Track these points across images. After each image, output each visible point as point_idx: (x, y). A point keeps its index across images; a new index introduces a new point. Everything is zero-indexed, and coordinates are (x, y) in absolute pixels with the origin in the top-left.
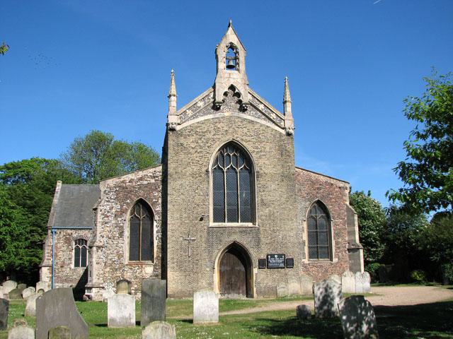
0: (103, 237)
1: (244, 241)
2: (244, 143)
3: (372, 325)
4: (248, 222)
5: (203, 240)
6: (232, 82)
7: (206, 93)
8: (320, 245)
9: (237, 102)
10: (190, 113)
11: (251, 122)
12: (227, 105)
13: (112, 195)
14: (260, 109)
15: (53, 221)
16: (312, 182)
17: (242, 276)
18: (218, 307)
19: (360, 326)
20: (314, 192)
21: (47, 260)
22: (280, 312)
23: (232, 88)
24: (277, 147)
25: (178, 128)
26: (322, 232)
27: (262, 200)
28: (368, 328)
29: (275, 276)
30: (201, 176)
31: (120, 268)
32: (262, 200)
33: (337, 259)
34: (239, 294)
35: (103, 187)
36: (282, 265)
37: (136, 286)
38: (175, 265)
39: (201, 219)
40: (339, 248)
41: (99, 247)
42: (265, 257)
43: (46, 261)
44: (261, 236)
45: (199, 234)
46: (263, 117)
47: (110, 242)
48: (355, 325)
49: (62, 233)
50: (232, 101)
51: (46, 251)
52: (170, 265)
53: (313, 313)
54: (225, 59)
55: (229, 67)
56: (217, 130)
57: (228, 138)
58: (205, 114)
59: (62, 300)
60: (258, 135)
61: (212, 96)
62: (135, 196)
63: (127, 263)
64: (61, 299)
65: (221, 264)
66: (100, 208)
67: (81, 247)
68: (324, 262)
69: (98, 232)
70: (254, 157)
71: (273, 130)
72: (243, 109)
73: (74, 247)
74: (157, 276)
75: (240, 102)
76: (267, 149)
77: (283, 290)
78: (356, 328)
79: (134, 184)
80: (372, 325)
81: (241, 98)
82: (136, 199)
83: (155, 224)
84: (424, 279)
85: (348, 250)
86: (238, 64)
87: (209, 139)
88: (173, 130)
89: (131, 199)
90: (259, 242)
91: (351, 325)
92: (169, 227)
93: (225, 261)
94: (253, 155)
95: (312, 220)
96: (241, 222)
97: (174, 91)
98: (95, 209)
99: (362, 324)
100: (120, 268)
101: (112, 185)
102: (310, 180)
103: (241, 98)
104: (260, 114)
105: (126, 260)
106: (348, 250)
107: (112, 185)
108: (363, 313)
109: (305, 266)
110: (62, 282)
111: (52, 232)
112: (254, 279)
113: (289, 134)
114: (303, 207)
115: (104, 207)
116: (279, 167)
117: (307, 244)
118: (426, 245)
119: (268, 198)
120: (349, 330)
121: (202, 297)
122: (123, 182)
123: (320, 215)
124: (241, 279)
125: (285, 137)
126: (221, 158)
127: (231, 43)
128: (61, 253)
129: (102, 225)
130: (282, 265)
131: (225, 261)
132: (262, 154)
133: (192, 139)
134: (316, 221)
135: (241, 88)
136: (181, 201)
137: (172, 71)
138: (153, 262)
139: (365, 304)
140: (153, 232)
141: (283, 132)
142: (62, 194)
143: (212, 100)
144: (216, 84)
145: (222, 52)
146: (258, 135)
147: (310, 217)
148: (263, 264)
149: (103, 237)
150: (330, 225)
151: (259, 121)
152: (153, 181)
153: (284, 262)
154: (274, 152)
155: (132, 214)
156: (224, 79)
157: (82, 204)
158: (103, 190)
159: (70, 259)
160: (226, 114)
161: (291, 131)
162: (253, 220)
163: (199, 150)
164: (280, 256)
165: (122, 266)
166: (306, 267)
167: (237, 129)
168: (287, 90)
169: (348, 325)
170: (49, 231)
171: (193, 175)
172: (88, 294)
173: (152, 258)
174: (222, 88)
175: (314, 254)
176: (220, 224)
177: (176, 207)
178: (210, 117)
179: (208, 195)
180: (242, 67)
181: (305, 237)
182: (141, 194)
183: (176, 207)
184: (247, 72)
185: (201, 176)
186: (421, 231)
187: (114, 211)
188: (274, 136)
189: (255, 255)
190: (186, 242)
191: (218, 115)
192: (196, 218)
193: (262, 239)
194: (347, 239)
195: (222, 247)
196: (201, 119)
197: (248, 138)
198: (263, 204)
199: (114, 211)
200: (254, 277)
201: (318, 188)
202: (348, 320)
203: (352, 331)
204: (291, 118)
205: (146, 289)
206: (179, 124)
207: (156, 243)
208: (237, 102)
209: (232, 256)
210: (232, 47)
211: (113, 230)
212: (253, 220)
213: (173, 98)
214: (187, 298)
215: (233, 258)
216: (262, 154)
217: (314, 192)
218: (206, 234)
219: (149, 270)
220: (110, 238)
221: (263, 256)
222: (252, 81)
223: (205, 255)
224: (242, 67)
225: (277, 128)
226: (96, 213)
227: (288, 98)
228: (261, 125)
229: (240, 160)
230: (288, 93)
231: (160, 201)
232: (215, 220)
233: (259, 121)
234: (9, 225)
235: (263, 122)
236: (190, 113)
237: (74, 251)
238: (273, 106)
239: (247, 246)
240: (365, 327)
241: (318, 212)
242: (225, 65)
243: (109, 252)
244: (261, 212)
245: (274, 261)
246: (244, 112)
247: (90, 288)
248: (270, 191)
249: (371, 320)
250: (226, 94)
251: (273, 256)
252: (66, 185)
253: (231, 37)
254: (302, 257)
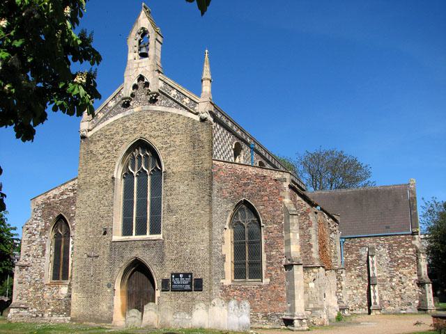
1: (147, 257)
6: (140, 72)
11: (162, 113)
14: (171, 96)
16: (238, 177)
20: (240, 190)
23: (141, 78)
24: (189, 139)
25: (89, 134)
27: (169, 206)
29: (180, 301)
32: (169, 206)
33: (268, 280)
37: (52, 307)
38: (78, 285)
39: (105, 233)
41: (22, 267)
42: (170, 277)
44: (166, 251)
46: (175, 104)
56: (125, 129)
57: (137, 136)
76: (178, 143)
77: (133, 319)
82: (56, 215)
90: (163, 259)
97: (207, 74)
104: (171, 101)
107: (40, 203)
109: (223, 288)
114: (224, 209)
116: (190, 163)
119: (175, 203)
122: (48, 198)
125: (200, 124)
127: (143, 28)
129: (29, 243)
130: (188, 287)
132: (171, 149)
133: (101, 144)
141: (197, 118)
145: (133, 41)
148: (166, 285)
149: (29, 256)
151: (170, 110)
153: (190, 283)
160: (136, 110)
163: (107, 155)
164: (186, 275)
166: (225, 290)
171: (100, 184)
177: (83, 221)
183: (83, 221)
188: (186, 125)
189: (158, 275)
191: (128, 112)
193: (167, 254)
195: (123, 265)
197: (157, 133)
198: (170, 210)
201: (245, 184)
206: (89, 130)
209: (142, 275)
214: (88, 323)
216: (171, 149)
217: (240, 190)
221: (167, 276)
222: (165, 67)
228: (173, 115)
233: (170, 110)
235: (175, 111)
244: (166, 221)
245: (179, 282)
246: (154, 103)
250: (135, 87)
251: (177, 275)
253: (144, 21)
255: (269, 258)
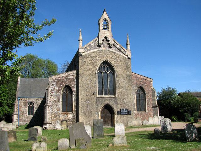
0: (51, 101)
1: (112, 103)
2: (111, 62)
3: (196, 135)
4: (112, 95)
5: (94, 103)
7: (95, 40)
8: (141, 105)
9: (108, 44)
10: (88, 48)
12: (104, 45)
13: (54, 83)
14: (117, 47)
15: (18, 94)
17: (110, 118)
18: (124, 130)
19: (192, 135)
21: (16, 112)
22: (145, 131)
23: (106, 38)
25: (83, 54)
26: (142, 100)
27: (118, 86)
28: (195, 136)
30: (93, 75)
31: (58, 115)
33: (148, 111)
34: (109, 126)
35: (50, 80)
36: (127, 113)
39: (93, 94)
40: (149, 106)
41: (49, 106)
42: (120, 110)
43: (15, 112)
45: (93, 100)
46: (119, 51)
47: (54, 104)
48: (190, 135)
49: (22, 99)
50: (106, 44)
51: (16, 108)
52: (80, 114)
53: (167, 130)
54: (102, 25)
55: (104, 29)
56: (99, 56)
57: (104, 59)
58: (94, 49)
59: (80, 128)
60: (116, 58)
61: (97, 41)
62: (64, 83)
63: (61, 113)
64: (79, 127)
65: (101, 113)
66: (49, 89)
67: (31, 106)
68: (143, 112)
69: (49, 99)
70: (115, 67)
71: (122, 56)
72: (110, 47)
73: (28, 106)
74: (74, 118)
75: (109, 44)
77: (130, 124)
78: (191, 136)
79: (64, 78)
80: (196, 135)
81: (109, 42)
83: (73, 96)
84: (177, 119)
85: (152, 107)
86: (108, 27)
87: (96, 59)
88: (81, 55)
89: (63, 85)
91: (189, 135)
92: (80, 97)
93: (103, 112)
94: (115, 67)
95: (138, 94)
96: (110, 95)
97: (81, 38)
98: (48, 89)
99: (193, 134)
100: (58, 115)
101: (54, 79)
102: (137, 77)
103: (109, 42)
104: (117, 49)
105: (61, 112)
106: (152, 107)
107: (54, 79)
108: (193, 130)
109: (135, 114)
110: (23, 121)
111: (18, 99)
112: (115, 119)
113: (129, 58)
114: (135, 89)
115: (51, 88)
117: (136, 104)
118: (178, 105)
120: (188, 136)
121: (118, 126)
122: (59, 77)
123: (141, 92)
124: (110, 119)
126: (101, 68)
127: (105, 18)
128: (22, 109)
131: (103, 112)
133: (89, 59)
134: (139, 95)
135: (109, 38)
136: (85, 86)
137: (80, 29)
138: (72, 112)
139: (193, 126)
140: (72, 99)
142: (21, 82)
143: (97, 43)
144: (99, 36)
145: (102, 22)
146: (116, 58)
147: (137, 93)
148: (119, 113)
149: (51, 101)
150: (72, 96)
152: (72, 77)
154: (123, 65)
155: (63, 92)
156: (102, 34)
157: (31, 87)
158: (50, 81)
159: (26, 111)
160: (103, 49)
161: (130, 57)
162: (114, 94)
163: (92, 64)
164: (126, 110)
165: (59, 114)
167: (108, 55)
168: (128, 40)
169: (188, 135)
170: (17, 99)
171: (90, 75)
172: (45, 126)
173: (72, 111)
174: (102, 38)
175: (139, 109)
176: (101, 96)
177: (83, 88)
178: (97, 50)
179: (96, 84)
180: (110, 29)
181: (135, 102)
182: (67, 83)
183: (83, 88)
184: (113, 31)
185: (93, 75)
186: (175, 99)
187: (55, 90)
188: (123, 59)
189: (116, 109)
190: (87, 104)
191: (100, 49)
192: (91, 93)
194: (152, 102)
195: (102, 106)
196: (93, 51)
197: (112, 60)
198: (119, 87)
199: (55, 90)
200: (115, 118)
202: (188, 133)
203: (189, 137)
204: (130, 51)
205: (95, 123)
206: (84, 53)
207: (74, 104)
208: (108, 44)
210: (105, 20)
211: (55, 99)
212: (114, 94)
213: (81, 41)
215: (106, 111)
217: (139, 83)
218: (95, 100)
219: (71, 116)
220: (54, 102)
221: (119, 110)
222: (114, 35)
223: (95, 109)
224: (110, 29)
225: (121, 54)
226: (48, 91)
227: (128, 43)
228: (118, 54)
229: (109, 69)
230: (128, 41)
231: (75, 86)
232: (99, 95)
234: (5, 96)
235: (119, 53)
236: (88, 48)
237: (28, 108)
238: (87, 43)
239: (112, 106)
240: (194, 136)
241: (140, 91)
242: (103, 28)
243: (53, 108)
244: (118, 91)
247: (46, 124)
248: (121, 82)
249: (196, 133)
250: (103, 40)
251: (123, 110)
252: (22, 78)
253: (105, 16)
254: (134, 110)
255: (148, 104)
